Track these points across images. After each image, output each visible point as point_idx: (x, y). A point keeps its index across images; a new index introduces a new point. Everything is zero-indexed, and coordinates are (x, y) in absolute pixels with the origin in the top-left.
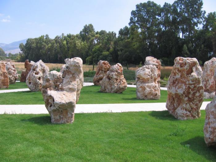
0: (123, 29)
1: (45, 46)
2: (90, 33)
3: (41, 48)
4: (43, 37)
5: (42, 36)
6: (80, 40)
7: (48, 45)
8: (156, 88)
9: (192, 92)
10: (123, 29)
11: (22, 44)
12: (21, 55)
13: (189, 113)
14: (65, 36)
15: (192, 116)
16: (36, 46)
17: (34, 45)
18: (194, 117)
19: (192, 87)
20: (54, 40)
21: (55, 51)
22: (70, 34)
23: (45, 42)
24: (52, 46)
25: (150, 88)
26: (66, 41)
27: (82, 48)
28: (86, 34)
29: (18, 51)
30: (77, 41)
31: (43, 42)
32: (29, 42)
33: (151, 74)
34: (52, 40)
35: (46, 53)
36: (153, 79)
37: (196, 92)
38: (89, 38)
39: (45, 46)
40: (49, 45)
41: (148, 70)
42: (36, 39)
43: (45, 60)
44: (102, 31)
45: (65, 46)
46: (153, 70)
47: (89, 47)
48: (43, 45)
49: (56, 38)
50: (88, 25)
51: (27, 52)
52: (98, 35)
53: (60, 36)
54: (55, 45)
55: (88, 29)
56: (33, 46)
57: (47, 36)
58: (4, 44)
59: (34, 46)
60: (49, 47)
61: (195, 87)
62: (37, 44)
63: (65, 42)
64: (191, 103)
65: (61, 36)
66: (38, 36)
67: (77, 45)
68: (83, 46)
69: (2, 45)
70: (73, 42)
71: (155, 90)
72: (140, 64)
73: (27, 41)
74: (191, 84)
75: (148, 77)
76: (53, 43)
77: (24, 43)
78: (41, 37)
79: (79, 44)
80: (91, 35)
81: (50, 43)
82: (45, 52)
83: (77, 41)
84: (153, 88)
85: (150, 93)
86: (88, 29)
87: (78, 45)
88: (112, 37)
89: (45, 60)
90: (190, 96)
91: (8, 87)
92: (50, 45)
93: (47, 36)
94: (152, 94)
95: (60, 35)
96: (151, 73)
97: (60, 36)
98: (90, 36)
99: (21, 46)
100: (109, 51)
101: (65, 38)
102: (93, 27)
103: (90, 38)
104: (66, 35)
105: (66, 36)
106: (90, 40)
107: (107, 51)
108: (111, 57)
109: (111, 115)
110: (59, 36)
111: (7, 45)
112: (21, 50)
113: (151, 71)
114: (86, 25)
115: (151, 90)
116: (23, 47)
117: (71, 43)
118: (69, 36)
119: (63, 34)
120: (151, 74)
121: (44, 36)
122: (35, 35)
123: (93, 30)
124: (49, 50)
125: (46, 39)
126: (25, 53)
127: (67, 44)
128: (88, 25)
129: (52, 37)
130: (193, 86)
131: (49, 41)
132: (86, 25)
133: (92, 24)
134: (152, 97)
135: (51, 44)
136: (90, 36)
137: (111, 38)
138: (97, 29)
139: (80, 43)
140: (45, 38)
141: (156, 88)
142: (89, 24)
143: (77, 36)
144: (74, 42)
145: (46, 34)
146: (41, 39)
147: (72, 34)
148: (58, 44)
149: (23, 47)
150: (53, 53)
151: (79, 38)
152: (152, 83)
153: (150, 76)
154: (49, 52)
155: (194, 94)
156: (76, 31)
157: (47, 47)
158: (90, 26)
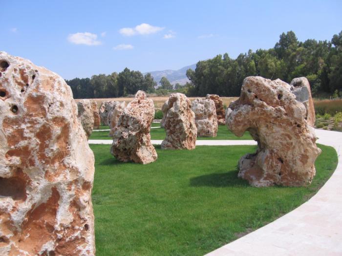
0: (338, 35)
1: (222, 71)
2: (291, 46)
3: (216, 75)
4: (219, 57)
5: (217, 56)
6: (275, 58)
7: (227, 68)
8: (208, 125)
9: (172, 125)
10: (338, 35)
11: (190, 70)
12: (188, 85)
13: (169, 144)
14: (254, 54)
15: (174, 146)
16: (209, 73)
17: (206, 71)
18: (176, 148)
19: (172, 120)
20: (236, 60)
21: (238, 77)
22: (260, 49)
23: (223, 66)
24: (234, 70)
25: (202, 125)
26: (255, 61)
27: (277, 71)
28: (283, 49)
29: (185, 81)
30: (270, 60)
31: (220, 65)
32: (200, 66)
33: (205, 110)
34: (234, 61)
35: (225, 81)
36: (207, 114)
37: (176, 125)
38: (289, 54)
39: (222, 71)
40: (229, 69)
41: (201, 105)
42: (210, 61)
43: (224, 92)
44: (308, 40)
45: (253, 69)
46: (207, 105)
47: (289, 67)
48: (219, 69)
49: (240, 56)
50: (286, 34)
51: (197, 81)
52: (302, 48)
53: (246, 53)
54: (238, 68)
55: (287, 40)
56: (205, 72)
57: (226, 55)
58: (171, 70)
59: (207, 72)
60: (229, 71)
61: (174, 120)
62: (211, 69)
63: (253, 63)
64: (173, 135)
65: (247, 54)
66: (212, 56)
67: (269, 67)
68: (280, 66)
69: (168, 73)
70: (264, 63)
71: (208, 127)
72: (334, 93)
73: (197, 65)
74: (171, 118)
75: (201, 112)
76: (235, 66)
77: (194, 69)
78: (217, 58)
79: (273, 64)
80: (292, 49)
81: (230, 65)
82: (224, 80)
83: (270, 60)
84: (205, 125)
85: (202, 130)
86: (287, 40)
87: (271, 65)
88: (324, 50)
89: (224, 92)
90: (171, 129)
91: (100, 127)
92: (230, 69)
93: (226, 55)
94: (204, 131)
95: (245, 51)
96: (204, 108)
97: (246, 53)
98: (290, 50)
99: (189, 74)
100: (317, 74)
101: (253, 57)
102: (294, 35)
103: (291, 54)
104: (254, 51)
105: (255, 52)
106: (289, 57)
107: (314, 74)
108: (320, 84)
109: (103, 145)
110: (244, 54)
111: (175, 72)
112: (190, 79)
113: (205, 106)
114: (283, 34)
115: (203, 127)
116: (191, 74)
117: (261, 63)
118: (260, 53)
119: (250, 51)
120: (205, 110)
121: (221, 56)
122: (208, 55)
123: (295, 40)
124: (229, 75)
125: (224, 60)
126: (195, 82)
127: (256, 65)
128: (286, 34)
129: (81, 78)
130: (172, 119)
131: (229, 63)
132: (283, 34)
133: (293, 31)
134: (204, 134)
135: (232, 67)
136: (290, 50)
137: (321, 52)
138: (302, 38)
139: (275, 63)
140: (223, 58)
141: (208, 125)
142: (288, 32)
143: (270, 52)
144: (266, 61)
145: (225, 53)
146: (217, 60)
147: (263, 49)
148: (242, 67)
149: (191, 74)
150: (236, 81)
151: (274, 55)
152: (205, 120)
153: (202, 111)
154: (229, 79)
155: (174, 127)
156: (269, 43)
157: (225, 72)
158: (290, 35)
